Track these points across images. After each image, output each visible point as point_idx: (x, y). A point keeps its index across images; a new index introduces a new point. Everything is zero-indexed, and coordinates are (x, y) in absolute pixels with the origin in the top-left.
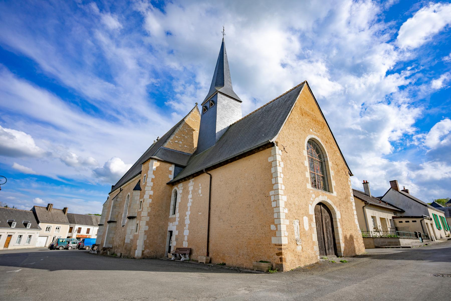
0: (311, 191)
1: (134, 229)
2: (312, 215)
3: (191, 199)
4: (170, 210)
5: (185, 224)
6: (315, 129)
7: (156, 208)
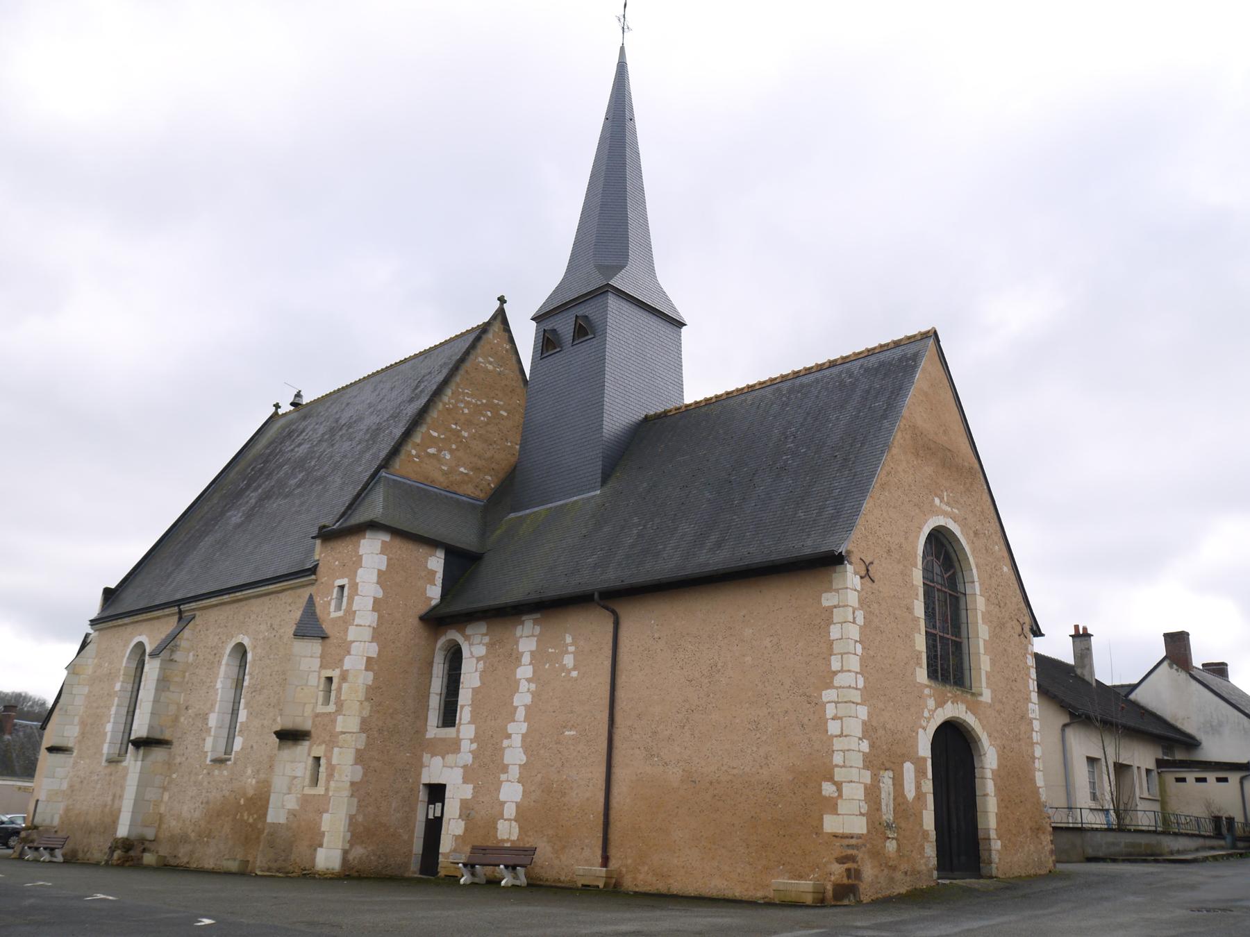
0: (927, 691)
1: (299, 773)
2: (925, 759)
3: (529, 680)
4: (428, 710)
5: (505, 762)
6: (948, 495)
7: (387, 702)
